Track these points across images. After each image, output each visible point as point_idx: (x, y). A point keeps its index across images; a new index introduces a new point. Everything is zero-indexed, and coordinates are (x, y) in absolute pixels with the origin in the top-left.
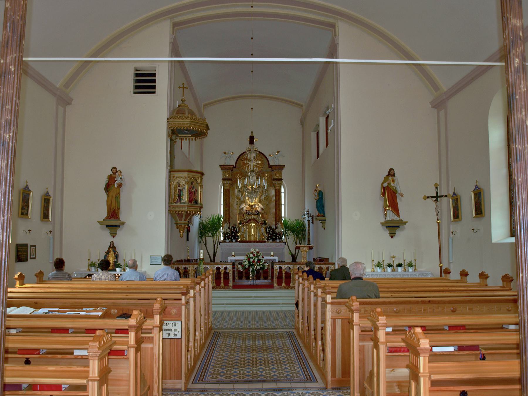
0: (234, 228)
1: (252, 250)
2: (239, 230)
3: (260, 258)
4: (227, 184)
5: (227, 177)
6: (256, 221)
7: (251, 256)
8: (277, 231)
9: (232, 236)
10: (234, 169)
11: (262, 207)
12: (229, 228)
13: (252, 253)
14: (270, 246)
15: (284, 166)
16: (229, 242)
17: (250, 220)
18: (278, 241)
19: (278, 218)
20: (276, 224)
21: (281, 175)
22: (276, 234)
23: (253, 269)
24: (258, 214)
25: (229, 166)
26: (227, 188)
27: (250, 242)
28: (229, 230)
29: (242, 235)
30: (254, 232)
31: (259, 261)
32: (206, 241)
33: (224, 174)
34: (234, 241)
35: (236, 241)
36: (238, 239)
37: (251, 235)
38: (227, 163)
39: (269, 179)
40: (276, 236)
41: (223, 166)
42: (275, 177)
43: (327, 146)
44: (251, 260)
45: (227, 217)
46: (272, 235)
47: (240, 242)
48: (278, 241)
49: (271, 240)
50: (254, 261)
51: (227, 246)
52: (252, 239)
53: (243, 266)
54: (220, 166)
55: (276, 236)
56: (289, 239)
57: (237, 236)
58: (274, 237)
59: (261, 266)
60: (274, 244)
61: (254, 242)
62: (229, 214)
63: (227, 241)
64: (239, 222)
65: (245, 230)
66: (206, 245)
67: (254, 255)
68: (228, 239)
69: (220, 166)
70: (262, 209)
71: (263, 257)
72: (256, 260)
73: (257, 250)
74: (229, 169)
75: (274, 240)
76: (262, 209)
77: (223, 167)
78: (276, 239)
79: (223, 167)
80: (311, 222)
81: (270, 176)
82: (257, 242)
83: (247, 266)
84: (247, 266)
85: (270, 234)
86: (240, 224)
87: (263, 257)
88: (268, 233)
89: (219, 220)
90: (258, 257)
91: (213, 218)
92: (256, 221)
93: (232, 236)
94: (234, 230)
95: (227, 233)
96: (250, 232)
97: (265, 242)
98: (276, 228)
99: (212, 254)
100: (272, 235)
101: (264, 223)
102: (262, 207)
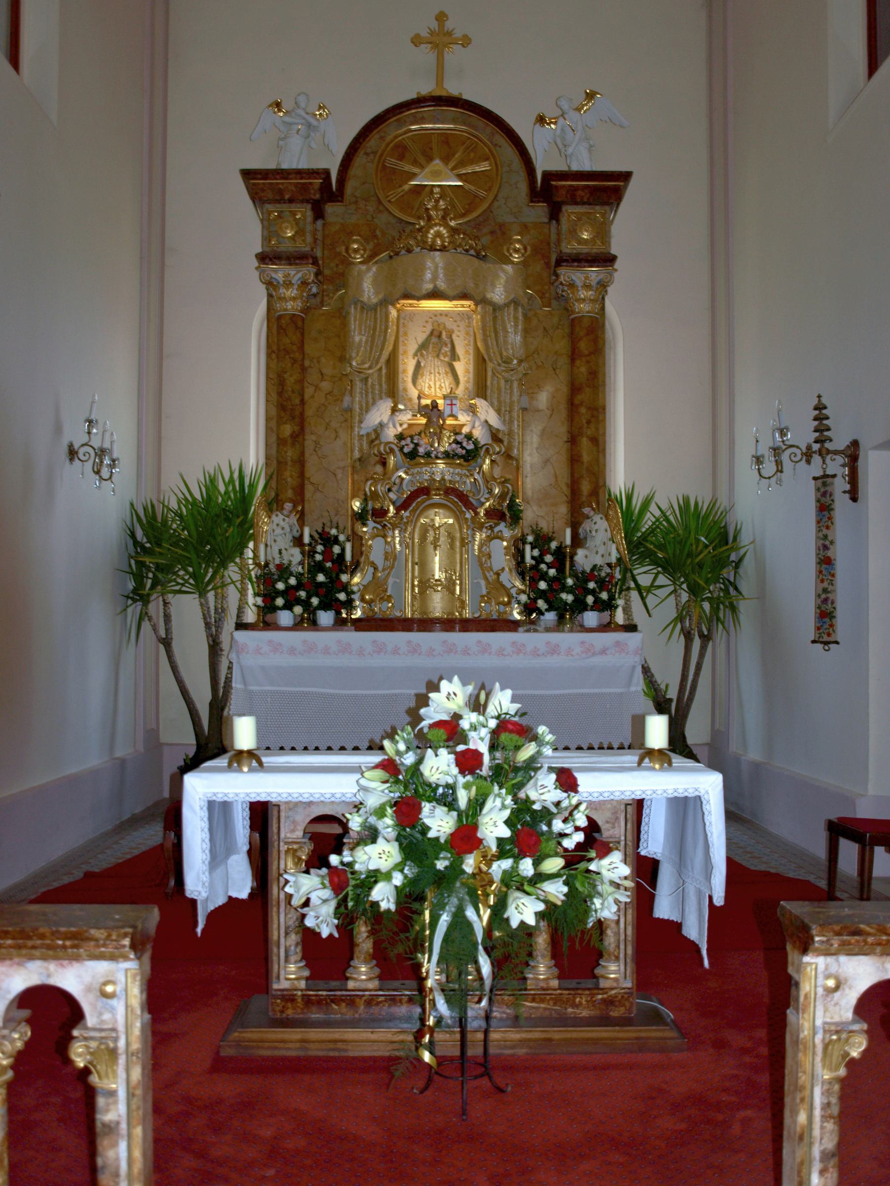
0: (329, 541)
1: (448, 699)
2: (358, 552)
3: (543, 791)
4: (288, 284)
5: (286, 247)
6: (463, 498)
7: (439, 766)
8: (584, 559)
9: (315, 589)
10: (331, 209)
11: (494, 420)
12: (298, 541)
13: (451, 731)
14: (554, 650)
15: (626, 176)
16: (297, 626)
17: (423, 491)
18: (591, 618)
19: (585, 487)
20: (575, 526)
21: (603, 232)
22: (582, 578)
23: (460, 923)
24: (468, 454)
25: (299, 173)
26: (292, 307)
27: (425, 624)
28: (295, 556)
29: (377, 587)
30: (447, 568)
31: (529, 831)
32: (167, 618)
33: (270, 230)
34: (325, 618)
35: (340, 623)
36: (349, 605)
37: (426, 584)
38: (295, 157)
39: (538, 267)
40: (581, 590)
41: (265, 174)
42: (570, 247)
43: (873, 67)
44: (439, 823)
45: (290, 476)
46: (557, 584)
47: (361, 625)
48: (591, 618)
49: (550, 617)
50: (466, 837)
51: (590, 651)
52: (437, 606)
53: (350, 888)
54: (248, 174)
55: (581, 590)
56: (656, 605)
57: (345, 588)
58: (569, 598)
59: (556, 890)
60: (568, 639)
61: (448, 624)
62: (301, 463)
63: (285, 618)
64: (356, 505)
65: (390, 556)
66: (166, 643)
67: (468, 762)
68: (288, 606)
69: (248, 174)
70: (495, 436)
71: (567, 781)
72: (494, 826)
73: (503, 701)
74: (300, 196)
75: (567, 616)
76: (495, 436)
77: (263, 185)
78: (580, 606)
79: (263, 185)
80: (840, 485)
81: (536, 251)
82: (467, 625)
83: (383, 896)
84: (383, 896)
85: (544, 576)
86: (361, 517)
87: (567, 781)
88: (529, 574)
89: (244, 500)
90: (511, 775)
91: (211, 483)
92: (459, 499)
93: (315, 589)
94: (327, 553)
95: (284, 571)
96: (423, 564)
97: (513, 626)
98: (578, 541)
99: (203, 697)
100: (557, 584)
101: (507, 513)
102: (494, 420)
